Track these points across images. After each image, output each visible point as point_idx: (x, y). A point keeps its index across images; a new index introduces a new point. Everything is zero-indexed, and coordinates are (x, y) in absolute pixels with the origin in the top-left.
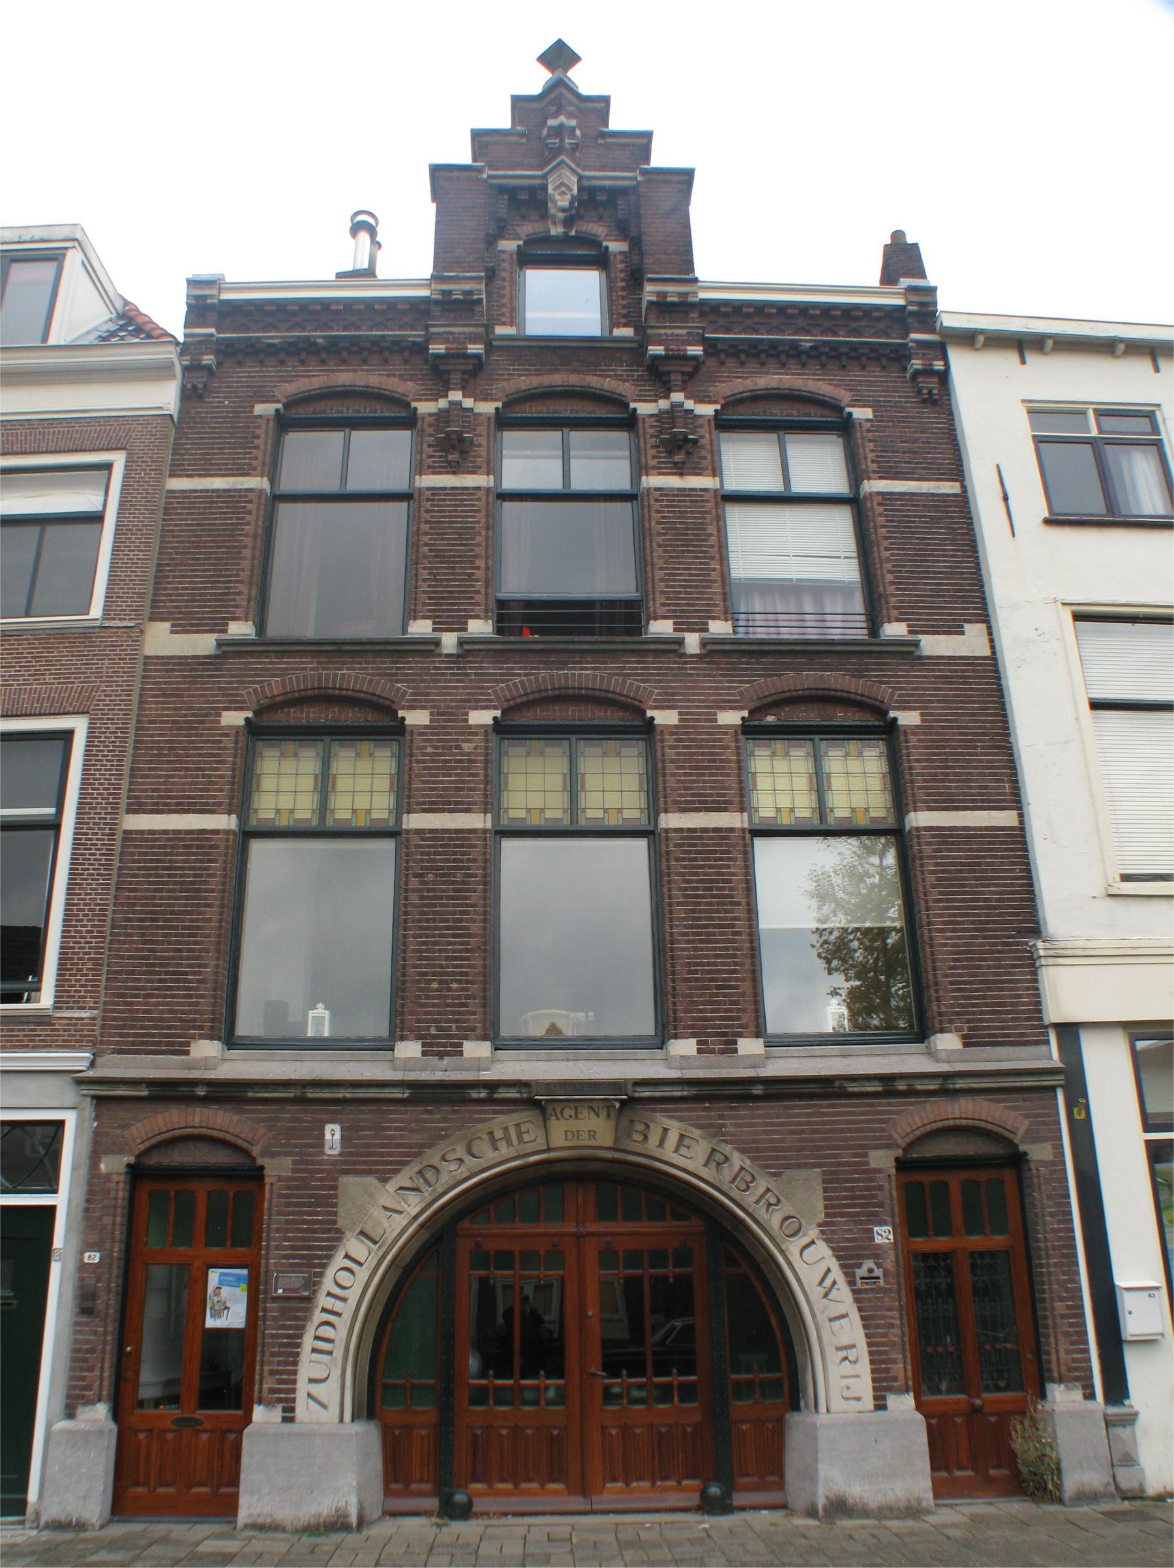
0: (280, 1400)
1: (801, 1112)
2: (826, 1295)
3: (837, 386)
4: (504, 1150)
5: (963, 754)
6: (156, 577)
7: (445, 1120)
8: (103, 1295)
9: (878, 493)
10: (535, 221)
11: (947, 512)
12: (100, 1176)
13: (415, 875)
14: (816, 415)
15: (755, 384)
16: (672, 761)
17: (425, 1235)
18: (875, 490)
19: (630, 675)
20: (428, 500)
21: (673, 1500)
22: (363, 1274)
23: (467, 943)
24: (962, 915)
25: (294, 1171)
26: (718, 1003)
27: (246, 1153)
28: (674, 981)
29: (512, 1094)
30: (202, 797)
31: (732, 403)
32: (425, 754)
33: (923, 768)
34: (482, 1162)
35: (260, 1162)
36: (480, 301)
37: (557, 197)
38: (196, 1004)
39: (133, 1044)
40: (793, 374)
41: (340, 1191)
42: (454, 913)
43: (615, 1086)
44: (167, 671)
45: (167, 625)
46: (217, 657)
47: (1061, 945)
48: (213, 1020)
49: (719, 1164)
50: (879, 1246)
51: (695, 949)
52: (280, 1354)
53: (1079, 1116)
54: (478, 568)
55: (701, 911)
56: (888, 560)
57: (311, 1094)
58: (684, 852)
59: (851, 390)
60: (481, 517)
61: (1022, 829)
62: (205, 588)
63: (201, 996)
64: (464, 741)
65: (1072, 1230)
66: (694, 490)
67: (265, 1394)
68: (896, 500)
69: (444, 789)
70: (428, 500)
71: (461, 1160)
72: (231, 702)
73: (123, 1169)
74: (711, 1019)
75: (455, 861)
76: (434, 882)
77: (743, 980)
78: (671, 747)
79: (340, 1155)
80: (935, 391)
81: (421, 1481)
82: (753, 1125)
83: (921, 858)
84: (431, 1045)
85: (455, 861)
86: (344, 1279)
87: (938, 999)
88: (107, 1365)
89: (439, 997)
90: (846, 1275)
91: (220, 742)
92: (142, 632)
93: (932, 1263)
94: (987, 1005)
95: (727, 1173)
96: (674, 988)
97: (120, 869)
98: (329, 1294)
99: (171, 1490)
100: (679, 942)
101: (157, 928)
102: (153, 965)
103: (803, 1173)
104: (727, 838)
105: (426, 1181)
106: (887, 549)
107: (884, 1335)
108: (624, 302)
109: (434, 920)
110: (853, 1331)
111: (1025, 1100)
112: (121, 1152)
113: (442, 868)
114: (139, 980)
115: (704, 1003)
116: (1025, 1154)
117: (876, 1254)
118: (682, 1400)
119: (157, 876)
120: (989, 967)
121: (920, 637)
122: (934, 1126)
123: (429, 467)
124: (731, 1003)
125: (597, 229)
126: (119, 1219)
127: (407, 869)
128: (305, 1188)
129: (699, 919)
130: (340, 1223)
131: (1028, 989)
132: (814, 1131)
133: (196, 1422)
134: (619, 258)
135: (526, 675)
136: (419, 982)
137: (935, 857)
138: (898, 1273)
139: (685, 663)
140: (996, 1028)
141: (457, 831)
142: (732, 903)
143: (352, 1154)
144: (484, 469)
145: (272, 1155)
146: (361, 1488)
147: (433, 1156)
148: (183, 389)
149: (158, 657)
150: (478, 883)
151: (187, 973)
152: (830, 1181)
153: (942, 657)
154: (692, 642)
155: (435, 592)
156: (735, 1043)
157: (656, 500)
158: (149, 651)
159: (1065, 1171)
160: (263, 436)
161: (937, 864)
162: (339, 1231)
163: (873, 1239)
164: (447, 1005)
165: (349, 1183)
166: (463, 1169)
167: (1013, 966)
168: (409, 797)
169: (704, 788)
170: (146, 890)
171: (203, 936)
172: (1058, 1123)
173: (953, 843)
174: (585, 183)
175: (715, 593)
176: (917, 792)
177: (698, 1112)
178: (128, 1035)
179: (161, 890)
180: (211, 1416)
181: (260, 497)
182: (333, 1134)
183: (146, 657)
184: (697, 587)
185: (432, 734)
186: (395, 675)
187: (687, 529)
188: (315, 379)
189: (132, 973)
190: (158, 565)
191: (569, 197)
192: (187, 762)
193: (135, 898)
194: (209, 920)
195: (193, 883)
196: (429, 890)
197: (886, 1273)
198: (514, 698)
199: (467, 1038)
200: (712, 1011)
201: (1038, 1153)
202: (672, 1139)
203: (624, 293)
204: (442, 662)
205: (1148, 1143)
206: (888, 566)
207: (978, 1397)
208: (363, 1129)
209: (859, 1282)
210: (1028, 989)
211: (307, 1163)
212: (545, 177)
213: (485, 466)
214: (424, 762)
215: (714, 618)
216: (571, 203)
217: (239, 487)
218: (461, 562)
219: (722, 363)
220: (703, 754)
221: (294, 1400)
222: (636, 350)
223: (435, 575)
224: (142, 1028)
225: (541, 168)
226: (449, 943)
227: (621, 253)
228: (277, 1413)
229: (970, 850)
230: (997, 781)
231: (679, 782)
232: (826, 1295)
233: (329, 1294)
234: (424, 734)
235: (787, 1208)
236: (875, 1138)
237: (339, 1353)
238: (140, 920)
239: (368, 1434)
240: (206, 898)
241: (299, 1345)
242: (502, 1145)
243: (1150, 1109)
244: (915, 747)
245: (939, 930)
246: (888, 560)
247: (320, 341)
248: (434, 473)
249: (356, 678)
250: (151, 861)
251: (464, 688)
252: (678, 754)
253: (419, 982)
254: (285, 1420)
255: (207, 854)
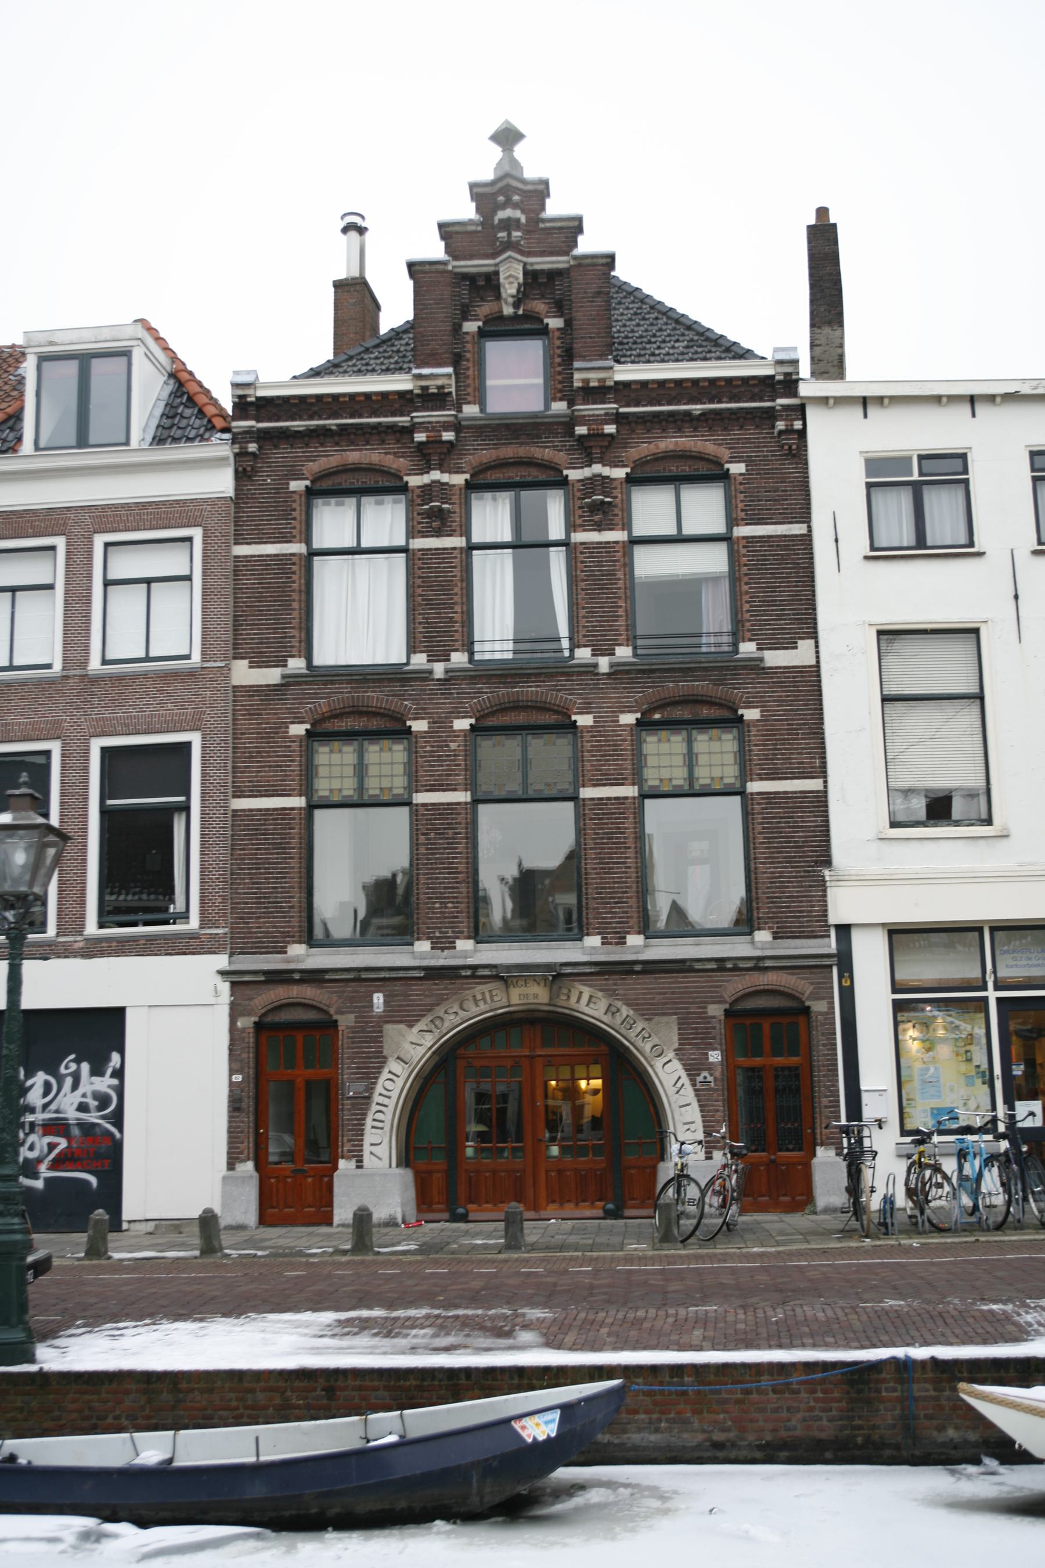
0: (354, 1156)
1: (665, 981)
2: (678, 1092)
3: (720, 445)
4: (483, 1007)
5: (788, 739)
6: (234, 626)
7: (446, 989)
8: (246, 1100)
9: (744, 538)
10: (491, 301)
11: (794, 550)
12: (238, 1030)
13: (423, 834)
14: (703, 468)
15: (657, 446)
16: (588, 751)
17: (436, 1058)
18: (741, 535)
19: (560, 690)
20: (420, 559)
21: (588, 1213)
22: (400, 1082)
23: (457, 878)
24: (778, 853)
25: (356, 1022)
26: (615, 913)
27: (326, 1012)
28: (587, 899)
29: (487, 972)
30: (281, 785)
31: (639, 464)
32: (425, 752)
33: (760, 750)
34: (469, 1014)
35: (335, 1017)
36: (450, 393)
37: (507, 286)
38: (289, 922)
39: (252, 948)
40: (687, 437)
41: (384, 1033)
42: (448, 858)
43: (548, 967)
44: (250, 696)
45: (246, 662)
46: (282, 685)
47: (841, 873)
48: (300, 932)
49: (613, 1013)
50: (712, 1063)
51: (601, 878)
52: (352, 1130)
53: (846, 983)
54: (456, 613)
55: (605, 853)
56: (747, 593)
57: (364, 975)
58: (595, 814)
59: (730, 448)
60: (457, 572)
61: (826, 792)
62: (269, 633)
63: (292, 917)
64: (451, 741)
65: (836, 1055)
66: (608, 543)
67: (345, 1153)
68: (757, 542)
69: (439, 775)
70: (420, 559)
71: (456, 1013)
72: (294, 718)
73: (251, 1025)
74: (610, 923)
75: (448, 824)
76: (435, 839)
77: (631, 898)
78: (588, 742)
79: (384, 1011)
80: (794, 447)
81: (439, 1203)
82: (636, 989)
83: (753, 814)
84: (437, 943)
85: (448, 824)
86: (389, 1085)
87: (758, 908)
88: (251, 1140)
89: (440, 913)
90: (691, 1080)
91: (290, 746)
92: (229, 669)
93: (750, 1074)
94: (791, 912)
95: (618, 1019)
96: (587, 904)
97: (232, 835)
98: (380, 1094)
99: (292, 1210)
100: (590, 874)
101: (261, 874)
102: (260, 898)
103: (665, 1019)
104: (623, 804)
105: (436, 1027)
106: (746, 584)
107: (713, 1116)
108: (560, 378)
109: (436, 863)
110: (694, 1113)
111: (811, 973)
112: (249, 1015)
113: (439, 829)
114: (251, 908)
115: (606, 913)
116: (809, 1007)
117: (710, 1067)
118: (594, 1155)
119: (257, 839)
120: (794, 887)
121: (765, 652)
122: (751, 990)
123: (419, 532)
124: (623, 912)
125: (539, 306)
126: (251, 1055)
127: (417, 830)
128: (363, 1032)
129: (604, 858)
130: (385, 1053)
131: (819, 901)
132: (673, 993)
133: (304, 1171)
134: (557, 334)
135: (491, 692)
136: (428, 903)
137: (762, 813)
138: (723, 1080)
139: (599, 680)
140: (795, 927)
141: (448, 804)
142: (626, 848)
143: (389, 1011)
144: (458, 533)
145: (342, 1013)
146: (403, 1205)
147: (440, 1011)
148: (236, 471)
149: (242, 687)
150: (462, 838)
151: (281, 902)
152: (683, 1024)
153: (780, 668)
154: (604, 664)
155: (427, 632)
156: (625, 938)
157: (582, 553)
158: (235, 682)
159: (834, 1018)
160: (298, 508)
161: (764, 818)
162: (385, 1057)
163: (707, 1059)
164: (445, 918)
165: (389, 1029)
166: (458, 1018)
167: (811, 886)
168: (417, 781)
169: (609, 770)
170: (251, 849)
171: (290, 878)
172: (832, 988)
173: (776, 803)
174: (529, 267)
175: (620, 626)
176: (753, 767)
177: (600, 981)
178: (247, 943)
179: (260, 849)
180: (313, 1168)
181: (300, 559)
182: (378, 999)
183: (234, 687)
184: (608, 621)
185: (430, 737)
186: (403, 695)
187: (603, 575)
188: (331, 458)
189: (247, 903)
190: (235, 616)
191: (516, 285)
192: (269, 762)
193: (245, 854)
194: (293, 868)
195: (281, 843)
196: (432, 844)
197: (715, 1080)
198: (483, 710)
199: (458, 938)
200: (611, 918)
201: (818, 1007)
202: (585, 998)
203: (559, 369)
204: (435, 685)
205: (894, 1001)
206: (746, 598)
207: (775, 1154)
208: (397, 996)
209: (698, 1085)
210: (819, 901)
211: (364, 1017)
212: (497, 265)
213: (458, 529)
214: (425, 757)
215: (619, 645)
216: (518, 291)
217: (285, 552)
218: (445, 608)
219: (633, 431)
220: (609, 746)
221: (362, 1156)
222: (569, 423)
223: (427, 618)
224: (257, 938)
225: (493, 256)
226: (445, 878)
227: (558, 329)
228: (353, 1164)
229: (787, 808)
230: (811, 758)
231: (592, 766)
232: (678, 1092)
233: (380, 1094)
234: (425, 737)
235: (655, 1040)
236: (712, 997)
237: (387, 1128)
238: (249, 869)
239: (407, 1175)
240: (289, 853)
241: (363, 1125)
242: (481, 1003)
243: (898, 977)
244: (755, 736)
245: (761, 863)
246: (747, 593)
247: (334, 428)
248: (423, 537)
249: (378, 698)
250: (252, 830)
251: (450, 703)
252: (593, 746)
253: (428, 903)
254: (358, 1167)
255: (288, 824)
